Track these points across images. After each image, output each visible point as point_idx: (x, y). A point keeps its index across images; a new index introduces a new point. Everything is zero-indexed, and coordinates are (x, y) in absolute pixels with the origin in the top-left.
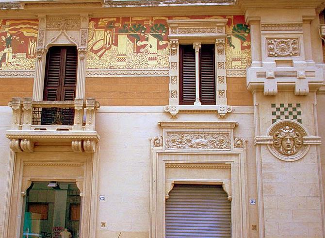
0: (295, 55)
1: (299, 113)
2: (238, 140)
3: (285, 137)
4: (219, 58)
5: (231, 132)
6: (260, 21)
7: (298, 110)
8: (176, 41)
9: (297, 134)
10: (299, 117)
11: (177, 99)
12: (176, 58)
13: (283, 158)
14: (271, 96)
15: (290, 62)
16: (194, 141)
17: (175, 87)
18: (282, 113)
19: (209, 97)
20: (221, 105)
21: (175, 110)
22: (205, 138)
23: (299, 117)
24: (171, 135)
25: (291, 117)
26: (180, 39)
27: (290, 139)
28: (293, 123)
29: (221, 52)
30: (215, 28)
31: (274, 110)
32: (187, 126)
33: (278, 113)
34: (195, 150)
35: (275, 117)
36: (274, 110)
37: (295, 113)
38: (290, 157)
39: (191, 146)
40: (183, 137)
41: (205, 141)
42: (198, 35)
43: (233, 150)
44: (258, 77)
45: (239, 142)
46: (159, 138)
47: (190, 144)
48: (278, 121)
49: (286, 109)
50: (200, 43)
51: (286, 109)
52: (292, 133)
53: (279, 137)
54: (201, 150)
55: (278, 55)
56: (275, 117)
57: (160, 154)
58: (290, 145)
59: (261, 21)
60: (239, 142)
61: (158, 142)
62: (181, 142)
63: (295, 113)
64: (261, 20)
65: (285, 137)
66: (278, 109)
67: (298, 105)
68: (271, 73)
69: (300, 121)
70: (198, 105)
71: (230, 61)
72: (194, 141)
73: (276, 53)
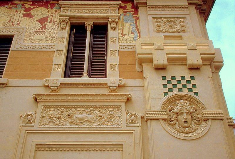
0: (184, 31)
1: (194, 86)
2: (132, 115)
3: (180, 111)
4: (111, 33)
5: (123, 105)
6: (146, 3)
7: (193, 82)
8: (66, 19)
9: (194, 108)
10: (194, 90)
11: (61, 70)
12: (66, 33)
13: (178, 135)
14: (160, 69)
15: (180, 37)
16: (77, 116)
17: (60, 60)
18: (175, 86)
19: (98, 68)
20: (113, 77)
21: (115, 83)
22: (91, 113)
23: (194, 90)
24: (47, 110)
25: (185, 90)
26: (70, 15)
27: (187, 113)
28: (188, 96)
29: (114, 29)
30: (108, 10)
31: (165, 82)
32: (69, 98)
33: (170, 86)
34: (74, 127)
35: (166, 90)
36: (165, 82)
37: (189, 86)
38: (189, 135)
39: (72, 123)
40: (62, 112)
41: (89, 116)
42: (90, 13)
43: (125, 127)
44: (142, 48)
45: (132, 118)
46: (33, 113)
47: (71, 120)
48: (171, 94)
49: (179, 82)
50: (92, 22)
51: (179, 82)
52: (188, 107)
53: (173, 112)
54: (86, 126)
55: (165, 32)
56: (166, 90)
57: (29, 132)
58: (187, 120)
59: (147, 3)
60: (132, 118)
61: (30, 117)
62: (59, 118)
63: (189, 86)
64: (147, 2)
65: (180, 111)
66: (169, 82)
67: (193, 78)
68: (159, 44)
69: (196, 93)
70: (85, 79)
71: (123, 37)
72: (77, 116)
73: (163, 30)
